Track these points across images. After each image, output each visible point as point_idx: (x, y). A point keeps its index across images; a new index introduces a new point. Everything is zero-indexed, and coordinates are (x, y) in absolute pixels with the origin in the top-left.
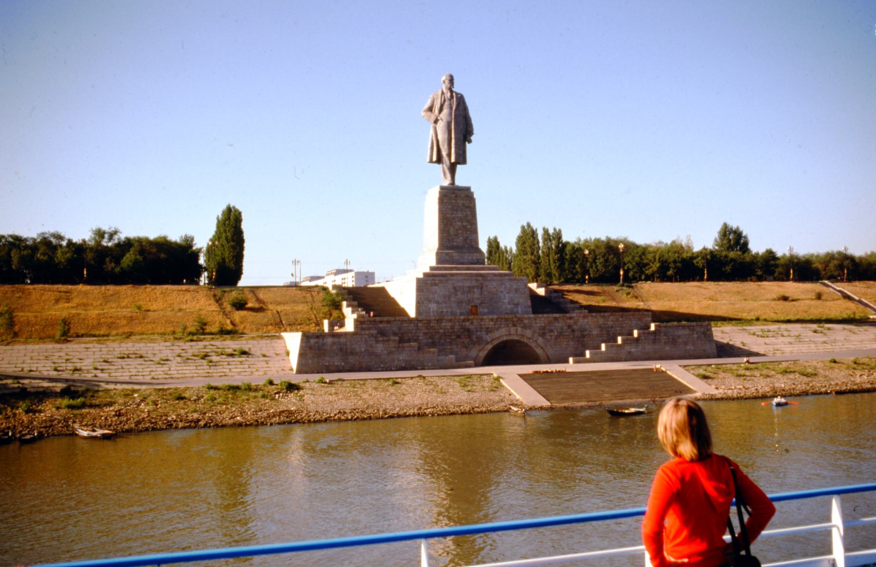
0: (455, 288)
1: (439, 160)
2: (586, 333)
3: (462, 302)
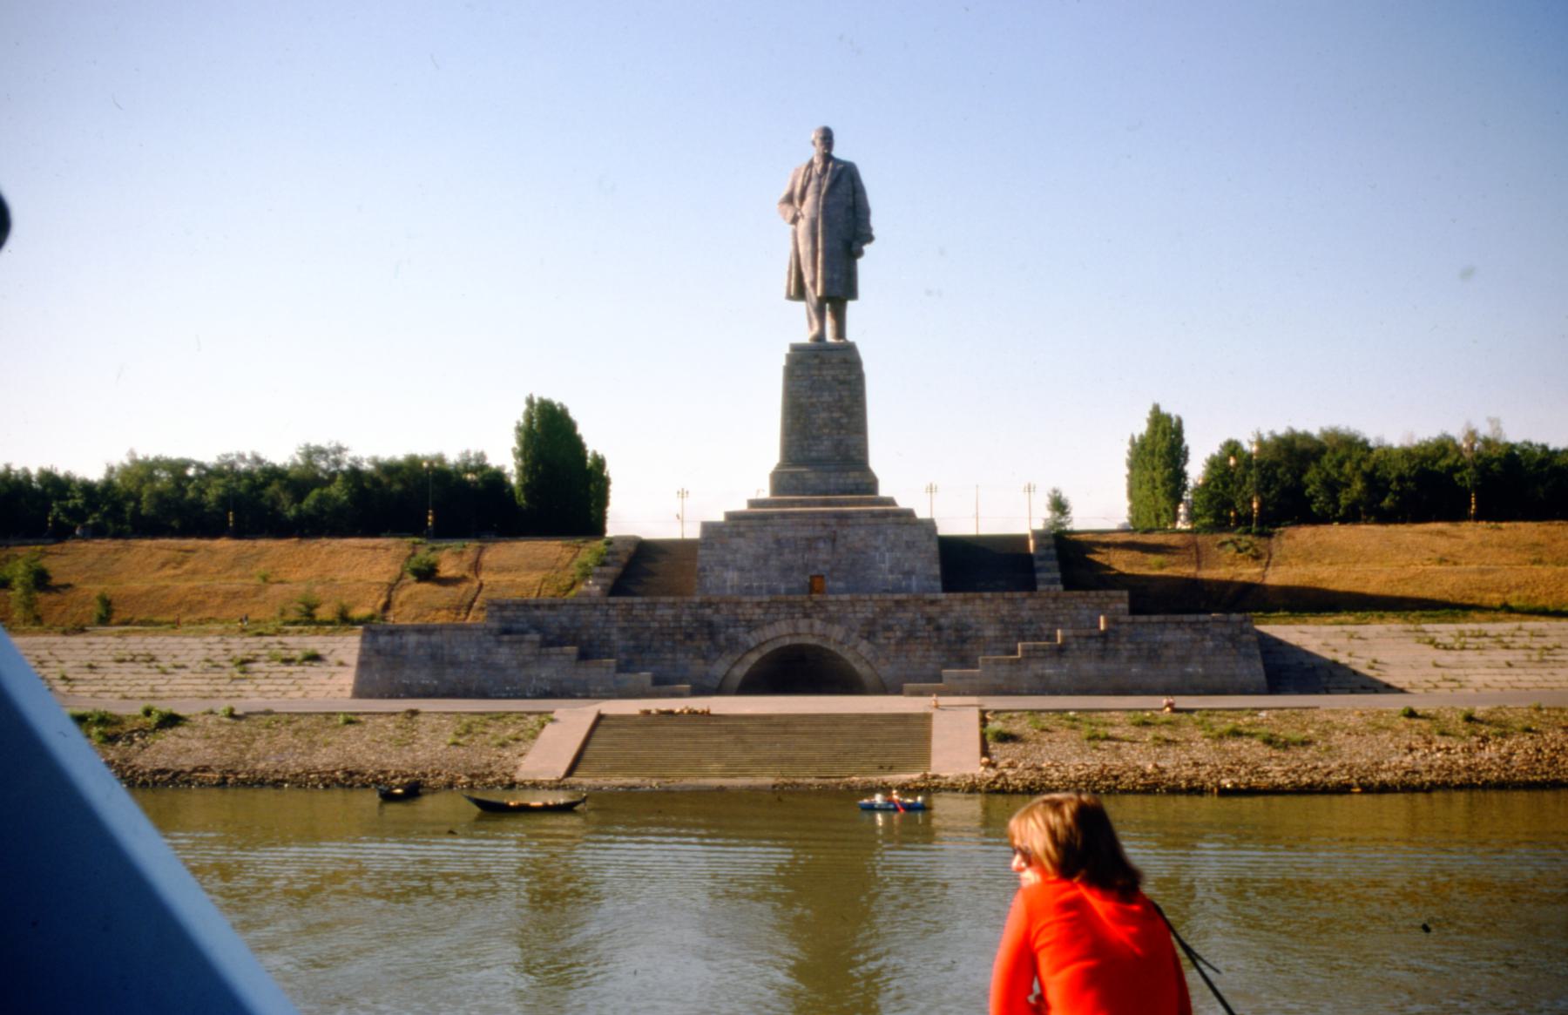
0: (778, 541)
1: (799, 293)
2: (970, 633)
3: (791, 569)
